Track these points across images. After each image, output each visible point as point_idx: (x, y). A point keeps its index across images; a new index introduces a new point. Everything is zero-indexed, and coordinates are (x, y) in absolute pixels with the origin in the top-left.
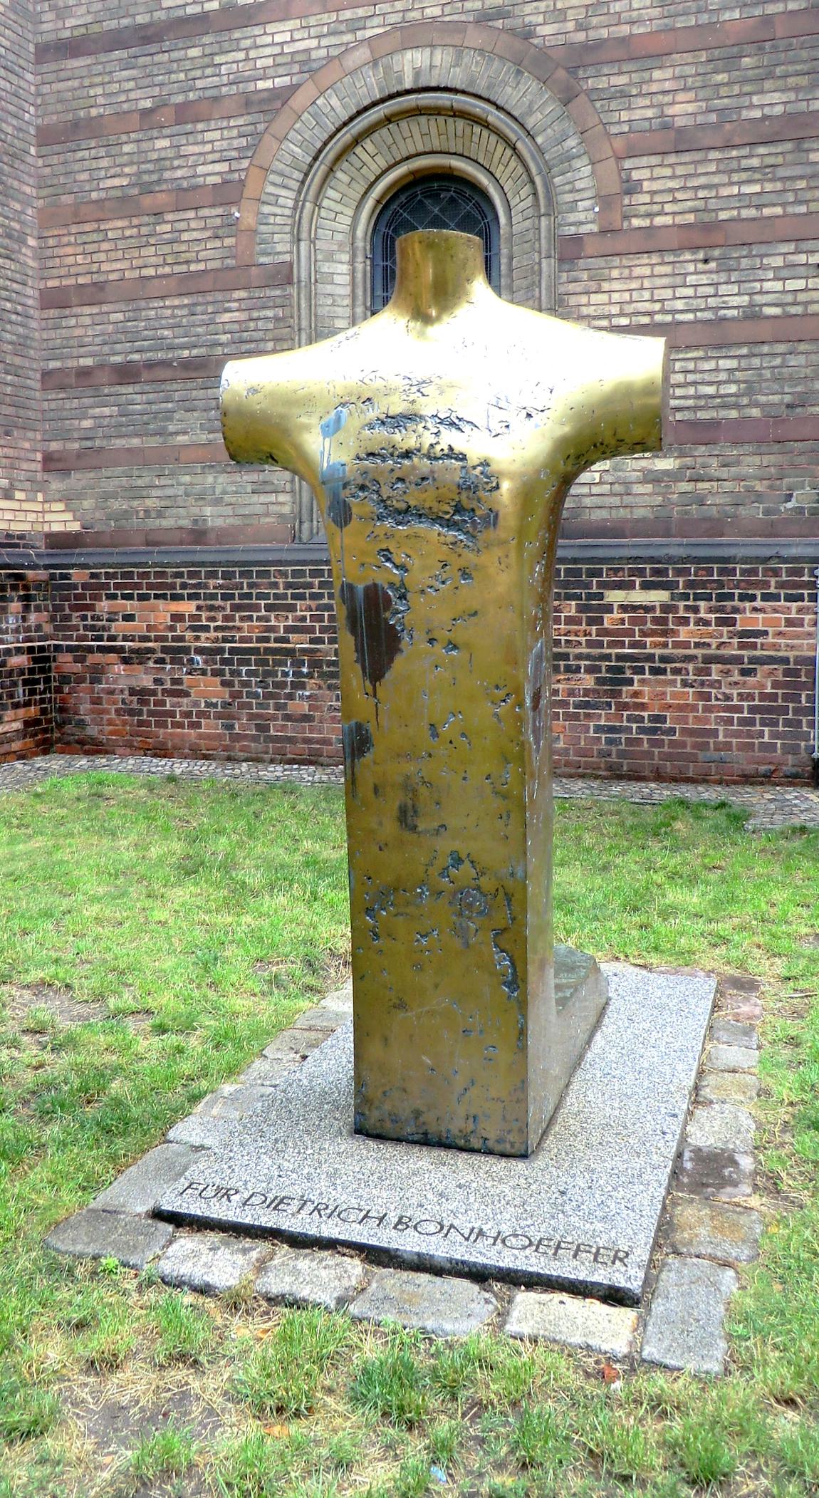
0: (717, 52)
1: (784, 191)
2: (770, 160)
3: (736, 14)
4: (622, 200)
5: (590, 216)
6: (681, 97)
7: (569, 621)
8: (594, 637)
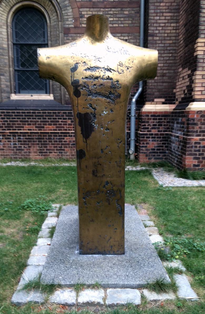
1: (118, 20)
2: (115, 12)
4: (80, 19)
5: (72, 23)
7: (69, 125)
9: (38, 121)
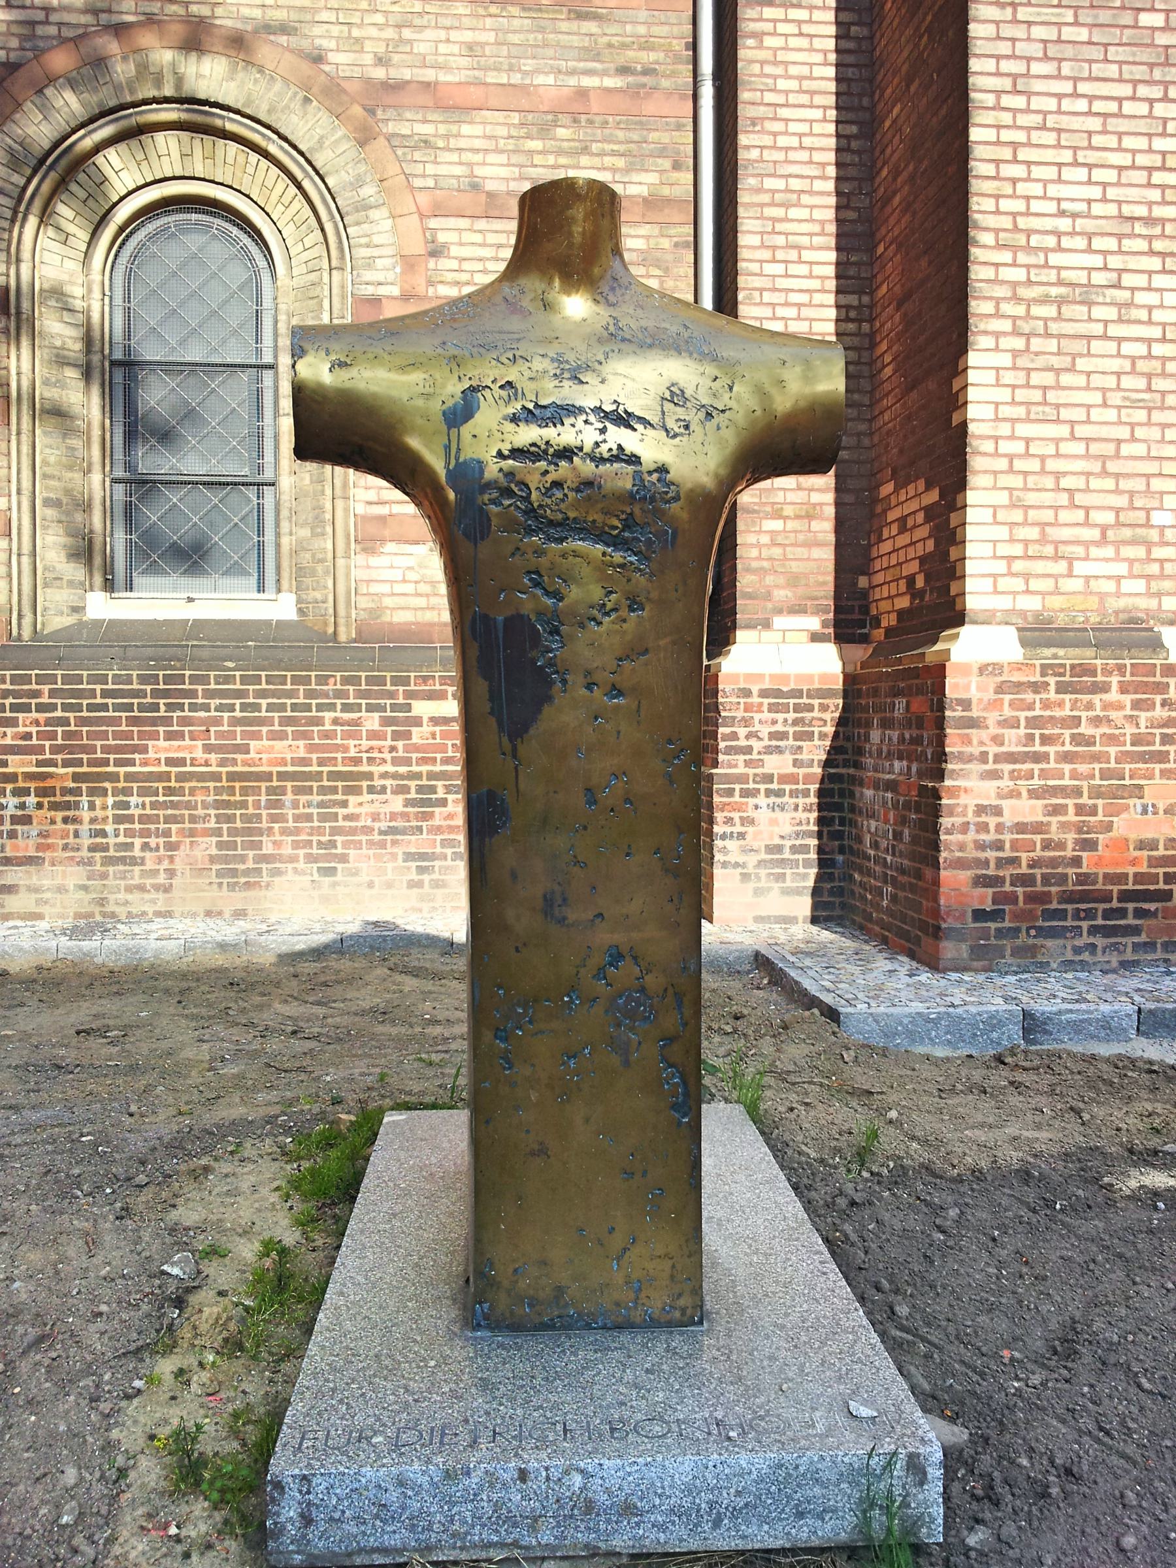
0: (530, 116)
3: (550, 80)
6: (491, 158)
7: (373, 735)
8: (401, 754)
9: (217, 722)
